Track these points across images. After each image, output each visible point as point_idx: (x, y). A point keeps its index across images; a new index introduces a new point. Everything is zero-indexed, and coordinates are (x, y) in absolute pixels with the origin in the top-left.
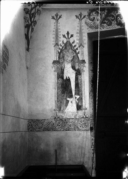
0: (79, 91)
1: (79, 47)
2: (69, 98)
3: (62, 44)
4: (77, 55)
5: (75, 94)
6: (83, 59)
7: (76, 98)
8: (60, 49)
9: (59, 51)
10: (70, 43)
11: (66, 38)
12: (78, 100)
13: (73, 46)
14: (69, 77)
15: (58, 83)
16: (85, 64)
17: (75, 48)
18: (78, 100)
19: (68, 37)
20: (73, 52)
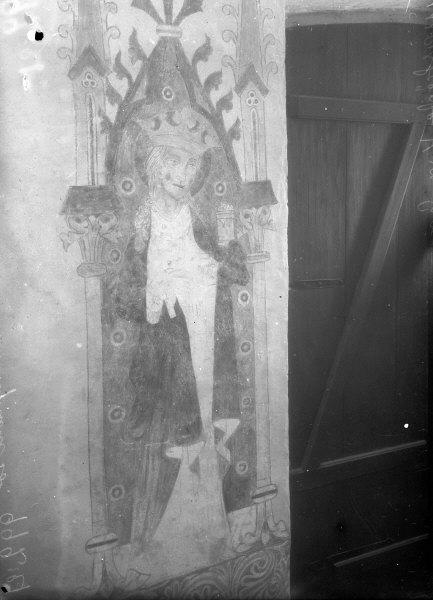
0: (237, 387)
1: (240, 87)
2: (180, 443)
3: (125, 61)
4: (228, 148)
5: (217, 412)
6: (262, 178)
7: (218, 434)
8: (112, 94)
9: (112, 111)
10: (181, 55)
11: (154, 15)
12: (230, 445)
13: (203, 79)
14: (177, 307)
15: (107, 352)
16: (273, 208)
17: (215, 96)
18: (230, 445)
19: (168, 11)
20: (205, 123)
